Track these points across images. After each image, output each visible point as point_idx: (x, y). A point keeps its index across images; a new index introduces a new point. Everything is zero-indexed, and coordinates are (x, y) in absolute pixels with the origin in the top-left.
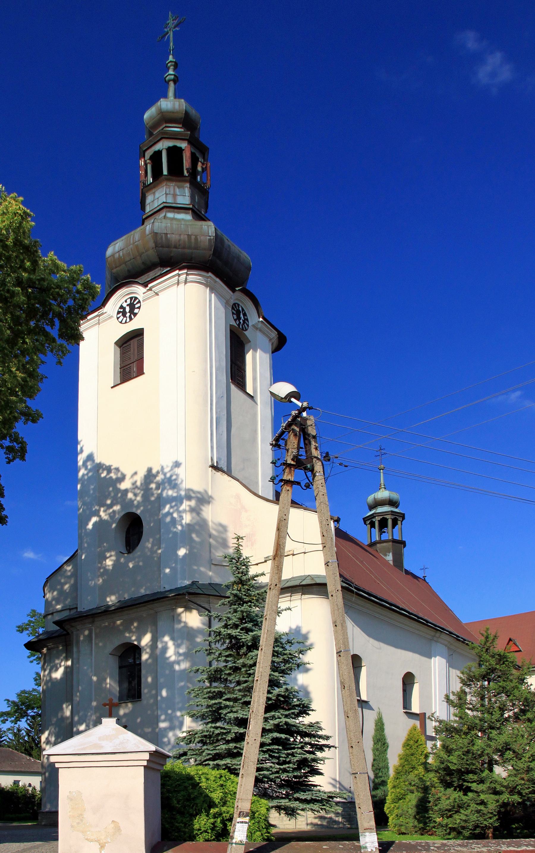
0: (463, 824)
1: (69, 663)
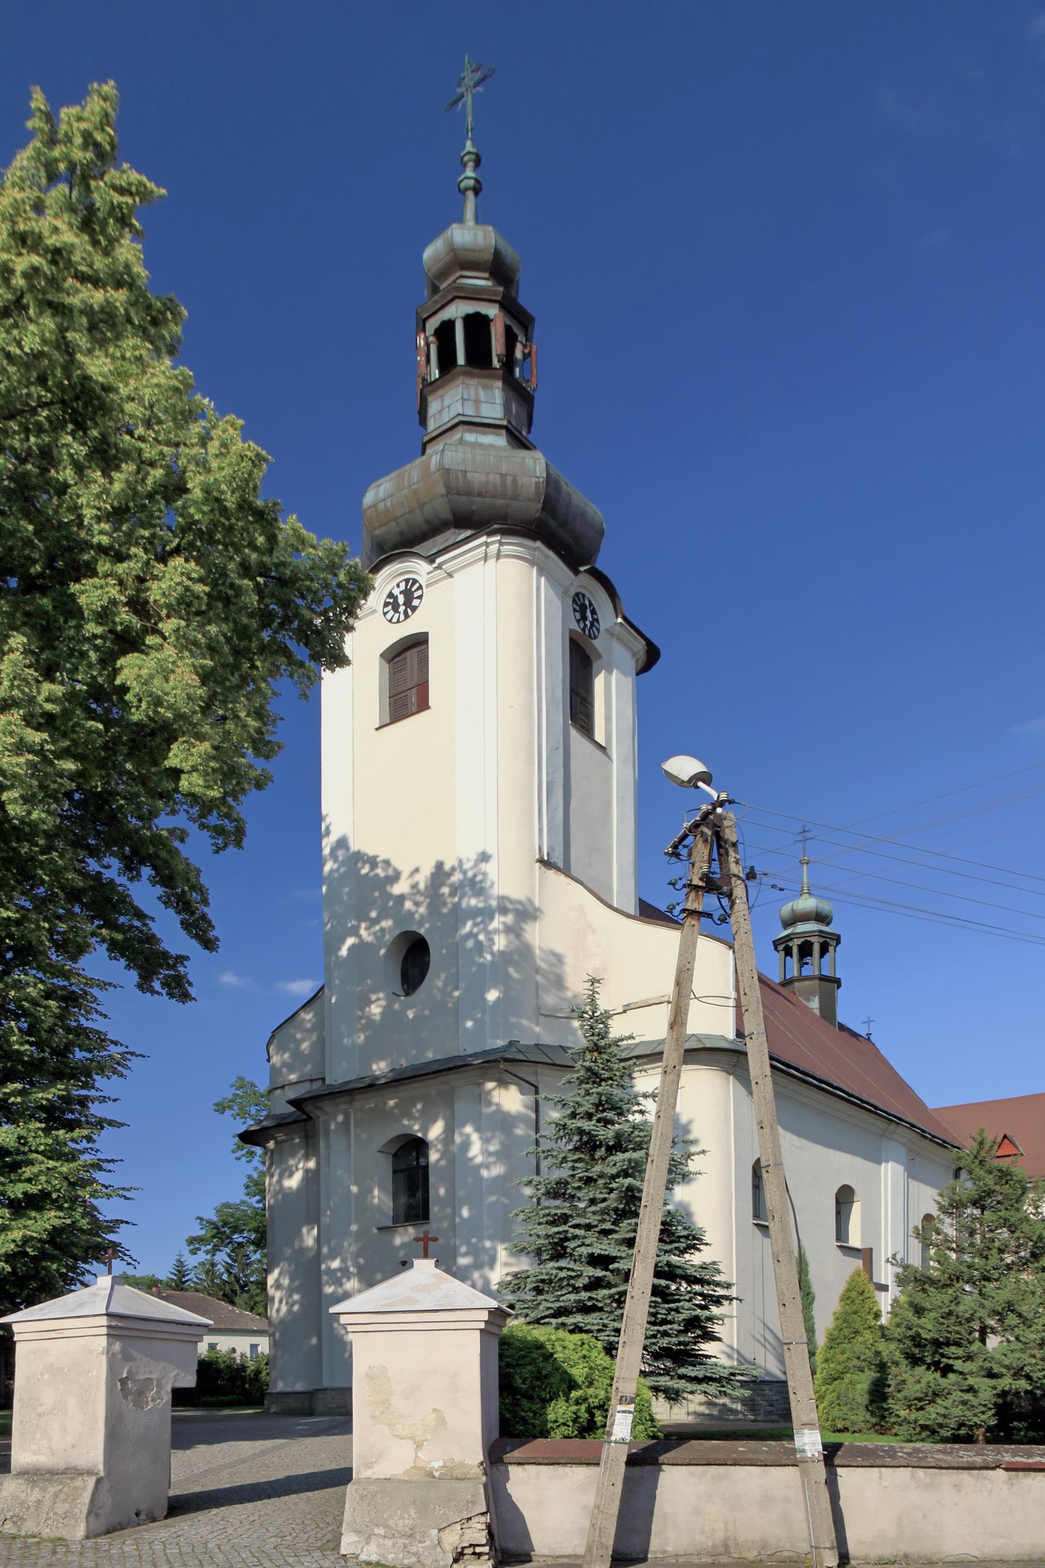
0: (940, 1420)
1: (312, 1164)
